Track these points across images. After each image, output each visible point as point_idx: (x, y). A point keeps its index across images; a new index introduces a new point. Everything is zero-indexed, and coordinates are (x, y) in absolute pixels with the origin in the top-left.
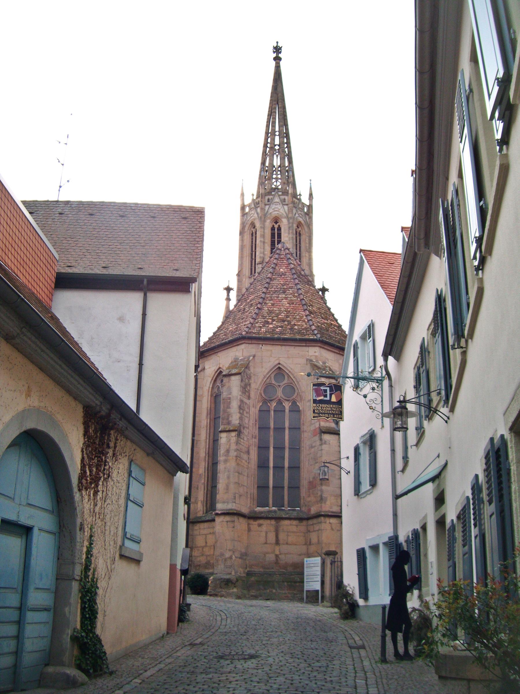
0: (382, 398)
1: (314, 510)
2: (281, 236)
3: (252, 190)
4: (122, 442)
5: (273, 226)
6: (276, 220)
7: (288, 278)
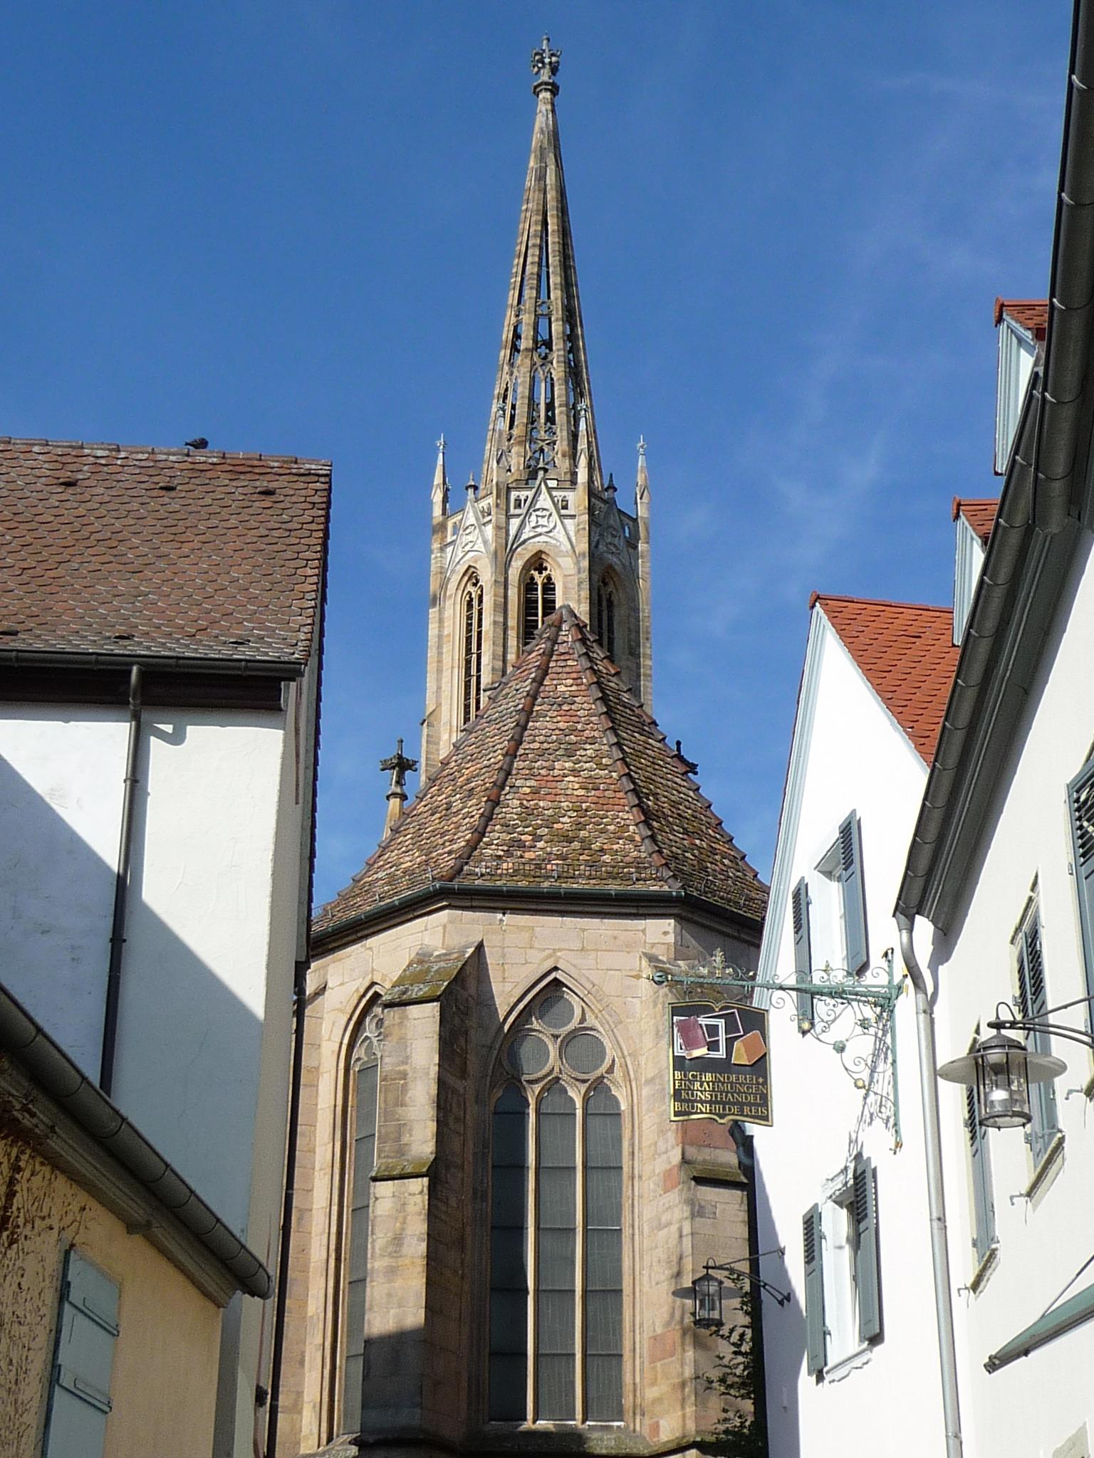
4: (37, 1180)
5: (532, 578)
6: (537, 562)
7: (580, 713)
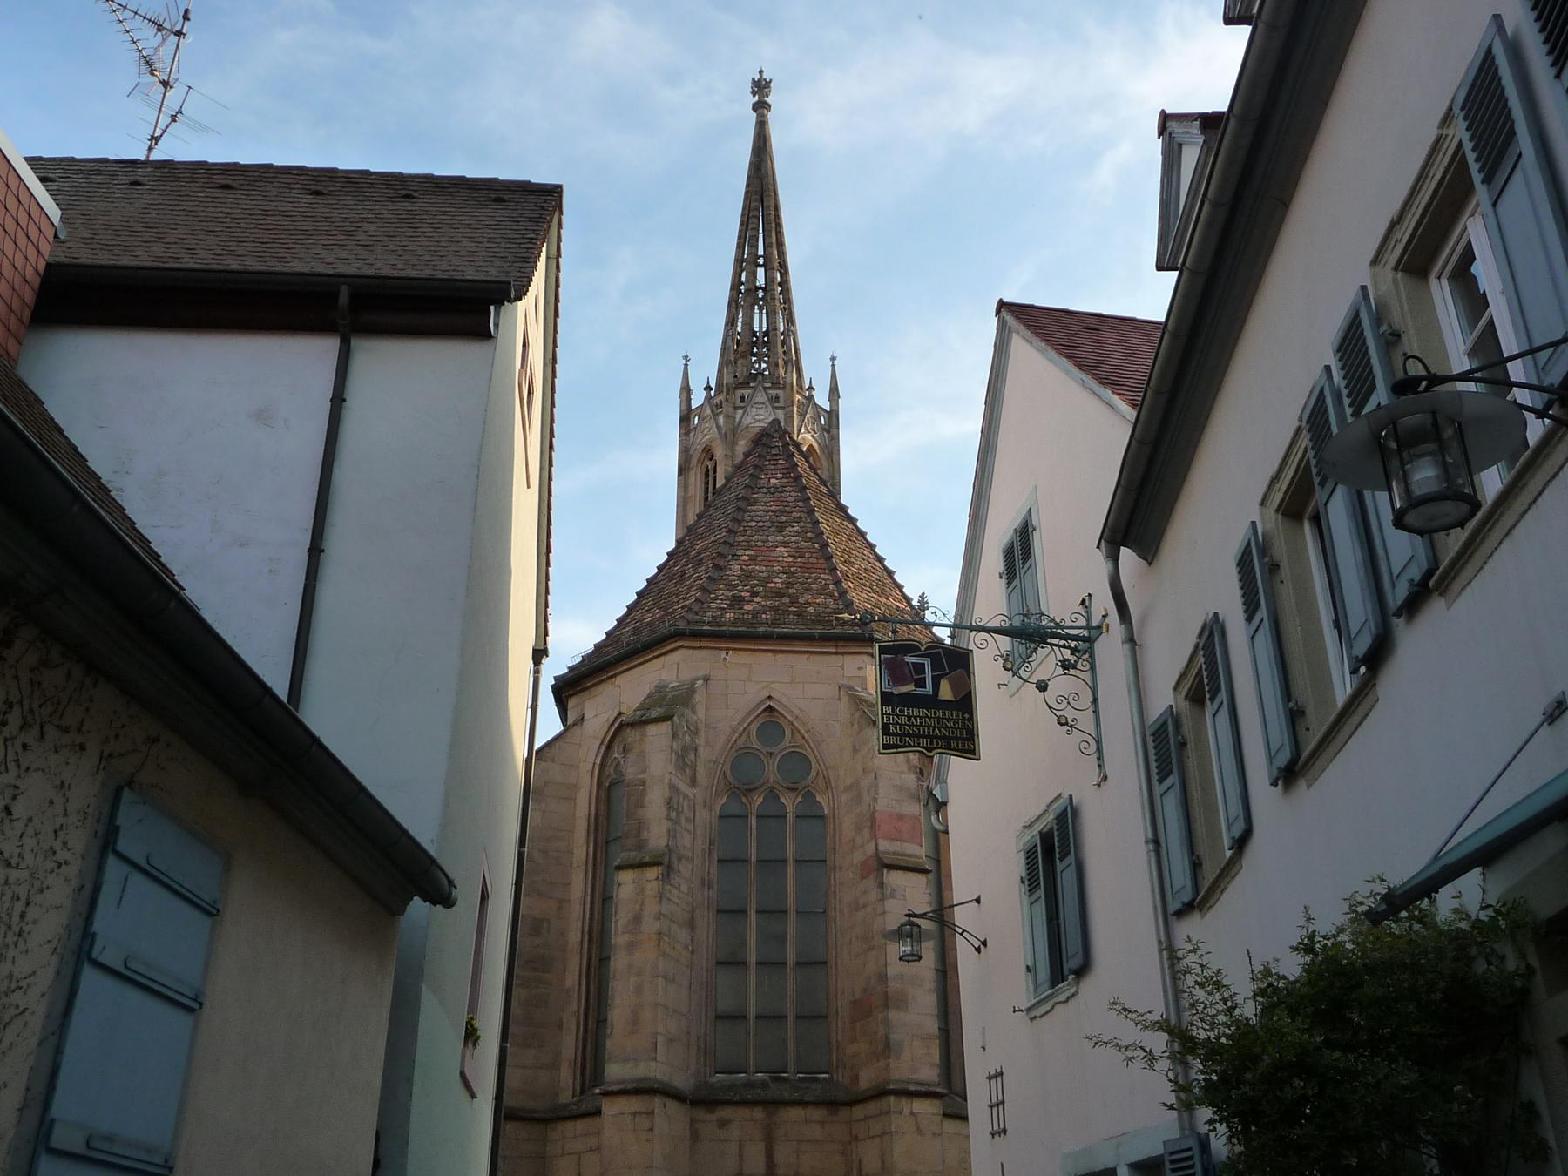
0: (1094, 691)
1: (867, 1079)
3: (706, 371)
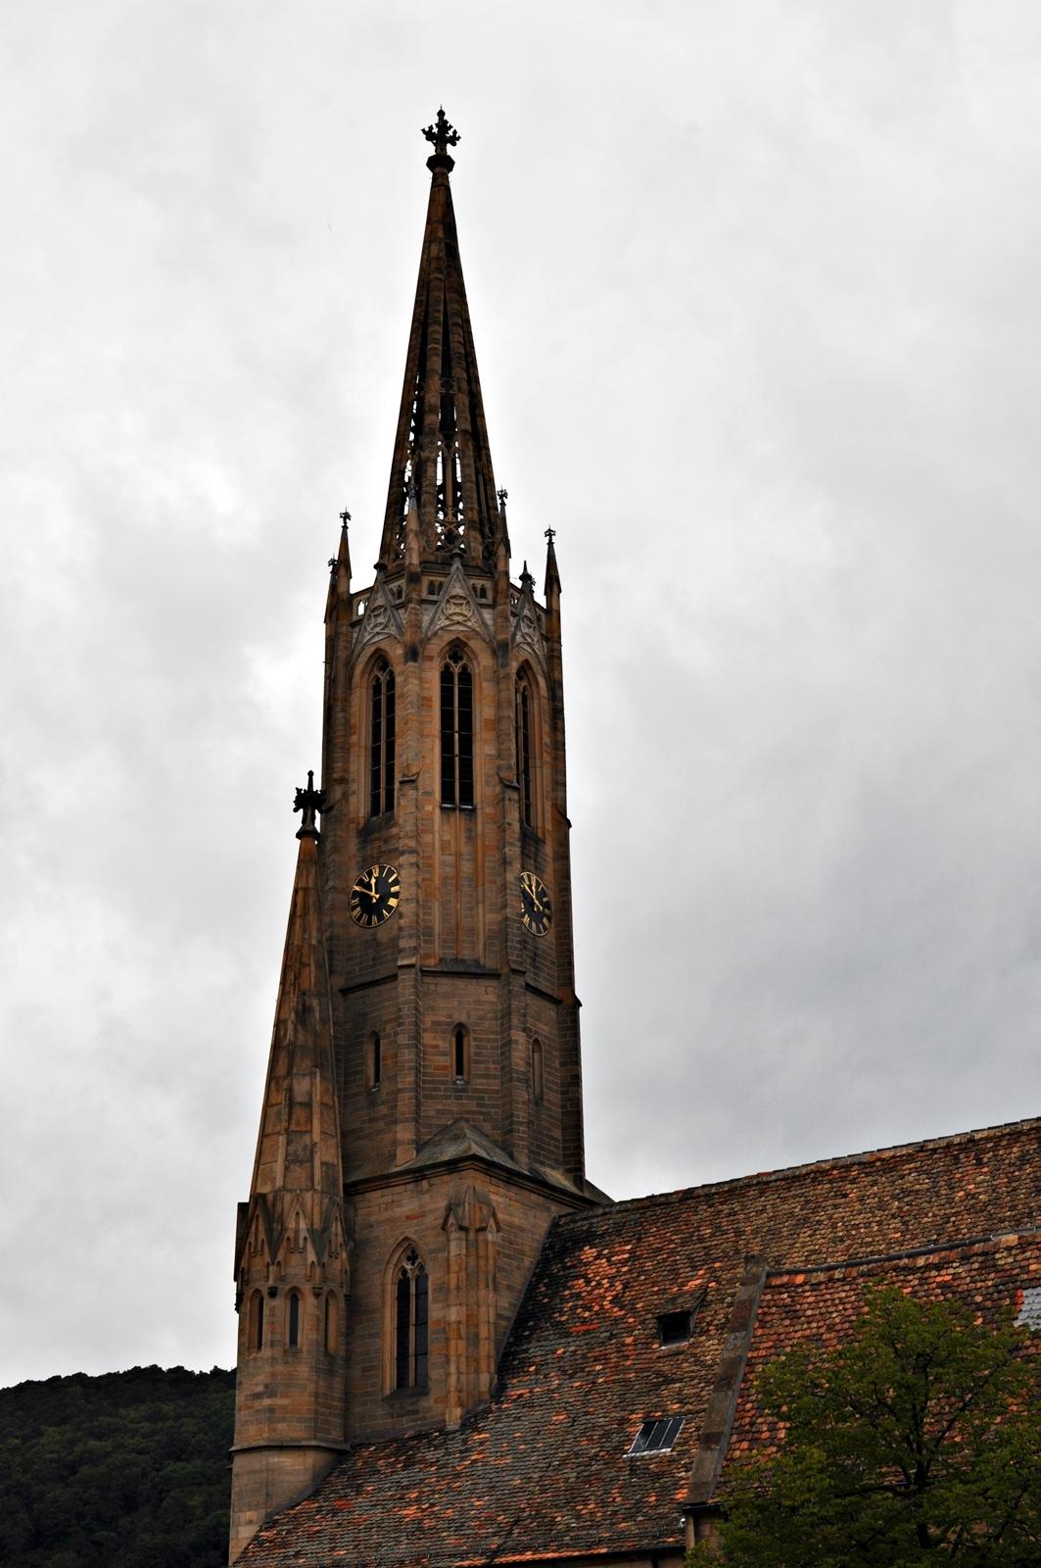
2: (470, 700)
6: (457, 649)
